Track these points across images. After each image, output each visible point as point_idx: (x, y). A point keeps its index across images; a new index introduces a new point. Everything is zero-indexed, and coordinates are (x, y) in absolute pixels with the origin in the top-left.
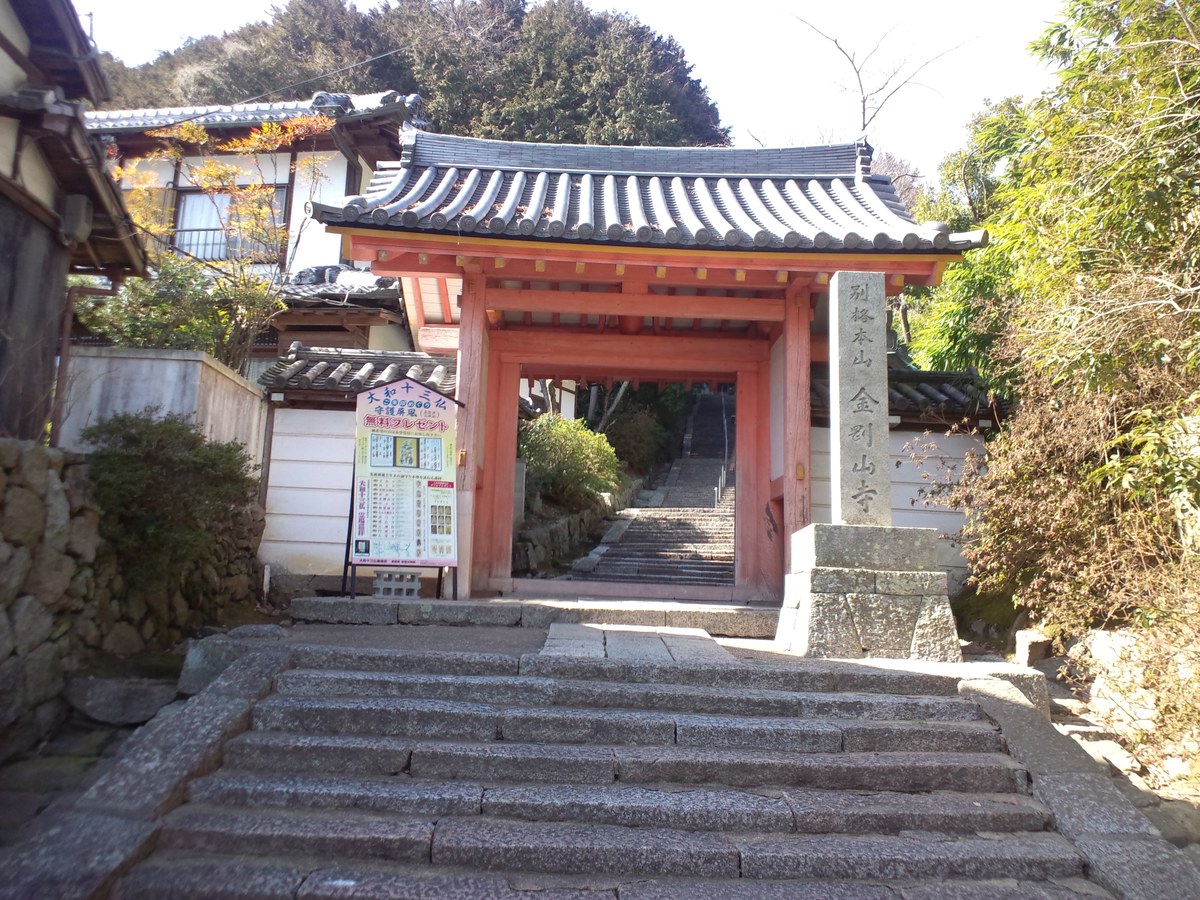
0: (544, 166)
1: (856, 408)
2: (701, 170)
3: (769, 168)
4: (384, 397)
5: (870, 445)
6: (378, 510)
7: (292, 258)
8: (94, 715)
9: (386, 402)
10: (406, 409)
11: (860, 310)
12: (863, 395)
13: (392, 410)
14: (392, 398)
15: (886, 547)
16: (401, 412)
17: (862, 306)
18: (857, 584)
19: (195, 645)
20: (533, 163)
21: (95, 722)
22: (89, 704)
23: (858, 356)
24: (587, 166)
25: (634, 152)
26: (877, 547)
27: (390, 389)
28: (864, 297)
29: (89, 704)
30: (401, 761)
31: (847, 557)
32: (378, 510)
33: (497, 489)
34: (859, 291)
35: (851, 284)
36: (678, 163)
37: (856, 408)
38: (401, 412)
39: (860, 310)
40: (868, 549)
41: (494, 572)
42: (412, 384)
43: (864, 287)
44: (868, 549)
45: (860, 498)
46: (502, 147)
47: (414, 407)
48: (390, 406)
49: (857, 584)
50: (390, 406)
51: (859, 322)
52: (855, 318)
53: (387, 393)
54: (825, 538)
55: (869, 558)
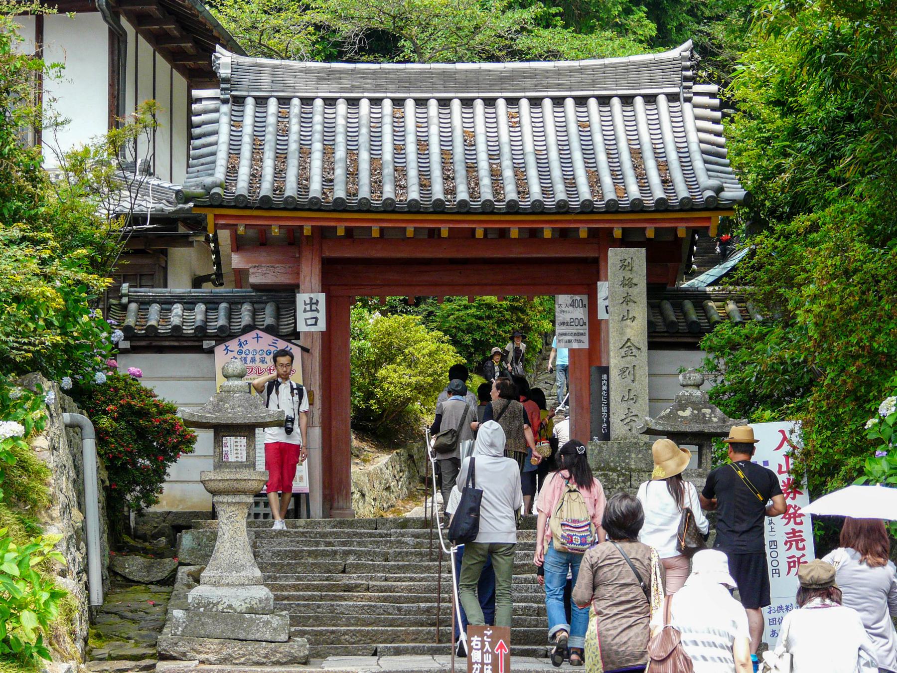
0: (365, 90)
1: (623, 354)
2: (524, 89)
3: (593, 84)
4: (238, 348)
5: (633, 381)
6: (239, 448)
7: (515, 489)
8: (131, 577)
9: (240, 352)
10: (258, 357)
11: (627, 278)
12: (629, 344)
13: (245, 359)
14: (245, 348)
15: (640, 456)
16: (253, 360)
17: (628, 275)
18: (618, 482)
19: (186, 533)
20: (353, 88)
21: (134, 581)
22: (127, 570)
23: (626, 314)
24: (407, 89)
25: (456, 72)
26: (633, 456)
27: (242, 341)
28: (630, 268)
29: (127, 570)
30: (341, 568)
31: (612, 464)
32: (239, 448)
33: (334, 423)
34: (626, 263)
35: (620, 258)
36: (503, 80)
37: (623, 354)
38: (253, 360)
39: (627, 278)
40: (626, 458)
41: (335, 505)
42: (261, 334)
43: (629, 260)
44: (626, 458)
45: (627, 421)
46: (319, 71)
47: (265, 355)
48: (243, 355)
49: (618, 482)
50: (243, 355)
51: (626, 288)
52: (623, 285)
53: (240, 345)
54: (596, 451)
55: (628, 464)
